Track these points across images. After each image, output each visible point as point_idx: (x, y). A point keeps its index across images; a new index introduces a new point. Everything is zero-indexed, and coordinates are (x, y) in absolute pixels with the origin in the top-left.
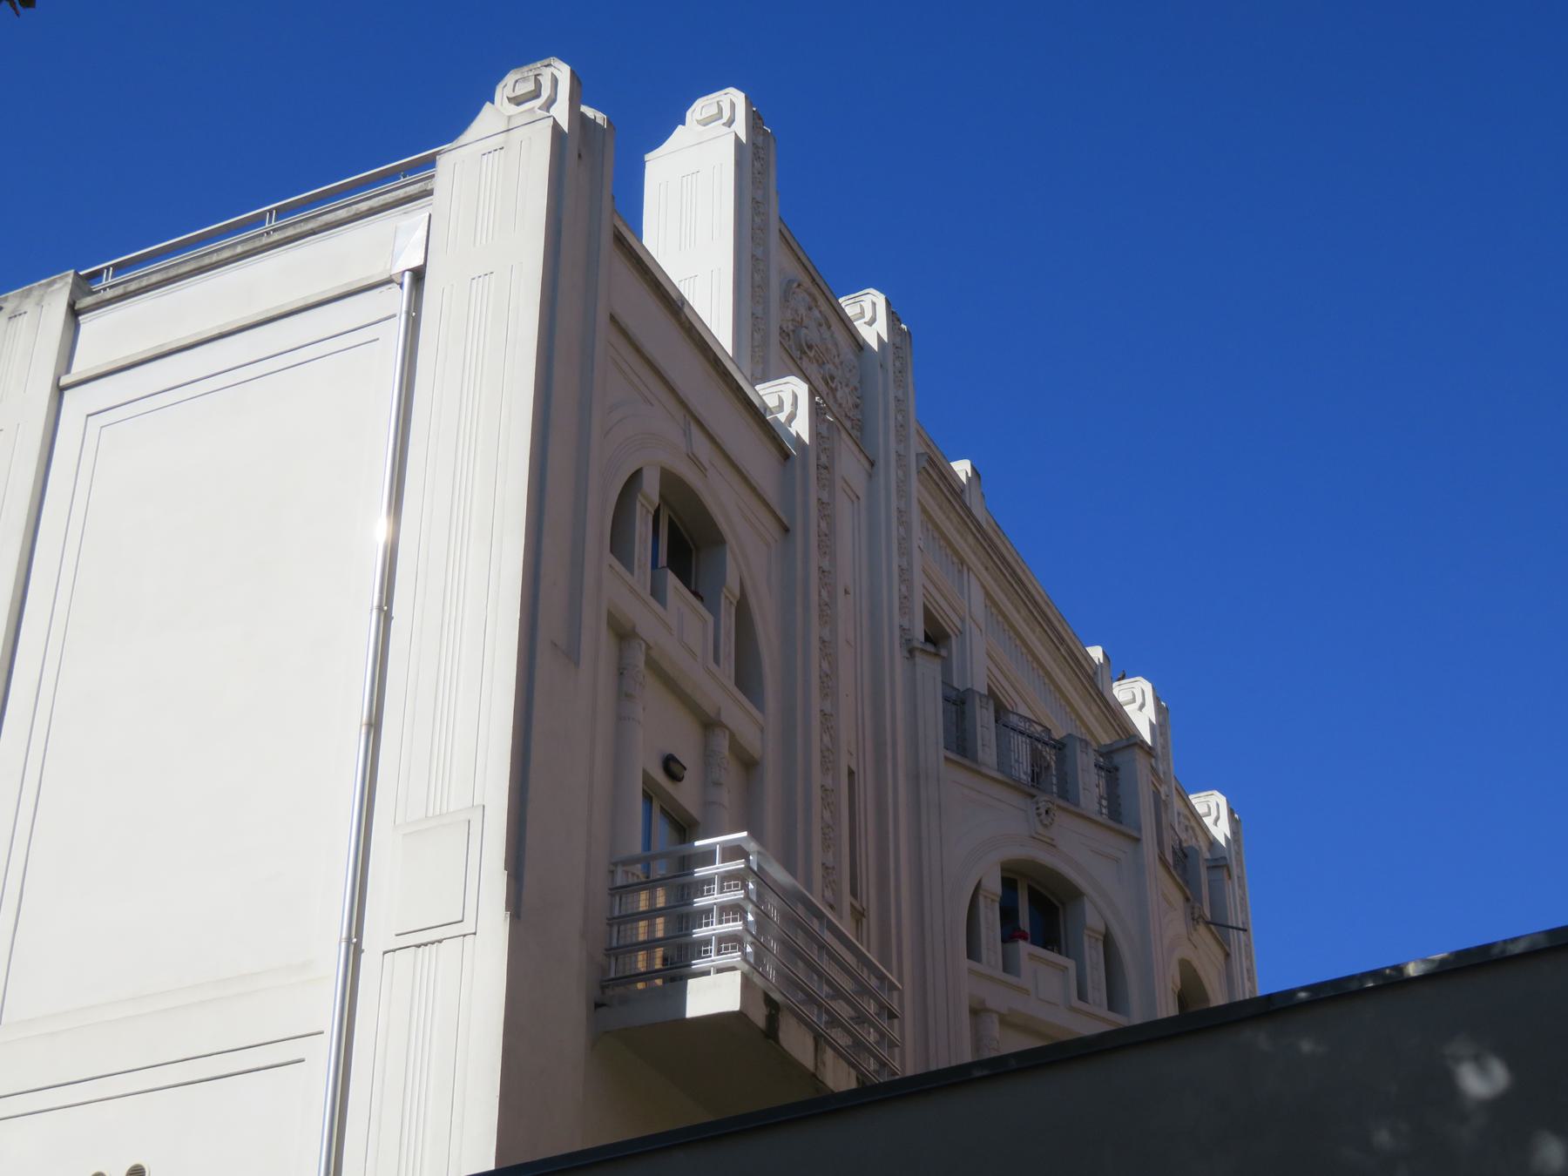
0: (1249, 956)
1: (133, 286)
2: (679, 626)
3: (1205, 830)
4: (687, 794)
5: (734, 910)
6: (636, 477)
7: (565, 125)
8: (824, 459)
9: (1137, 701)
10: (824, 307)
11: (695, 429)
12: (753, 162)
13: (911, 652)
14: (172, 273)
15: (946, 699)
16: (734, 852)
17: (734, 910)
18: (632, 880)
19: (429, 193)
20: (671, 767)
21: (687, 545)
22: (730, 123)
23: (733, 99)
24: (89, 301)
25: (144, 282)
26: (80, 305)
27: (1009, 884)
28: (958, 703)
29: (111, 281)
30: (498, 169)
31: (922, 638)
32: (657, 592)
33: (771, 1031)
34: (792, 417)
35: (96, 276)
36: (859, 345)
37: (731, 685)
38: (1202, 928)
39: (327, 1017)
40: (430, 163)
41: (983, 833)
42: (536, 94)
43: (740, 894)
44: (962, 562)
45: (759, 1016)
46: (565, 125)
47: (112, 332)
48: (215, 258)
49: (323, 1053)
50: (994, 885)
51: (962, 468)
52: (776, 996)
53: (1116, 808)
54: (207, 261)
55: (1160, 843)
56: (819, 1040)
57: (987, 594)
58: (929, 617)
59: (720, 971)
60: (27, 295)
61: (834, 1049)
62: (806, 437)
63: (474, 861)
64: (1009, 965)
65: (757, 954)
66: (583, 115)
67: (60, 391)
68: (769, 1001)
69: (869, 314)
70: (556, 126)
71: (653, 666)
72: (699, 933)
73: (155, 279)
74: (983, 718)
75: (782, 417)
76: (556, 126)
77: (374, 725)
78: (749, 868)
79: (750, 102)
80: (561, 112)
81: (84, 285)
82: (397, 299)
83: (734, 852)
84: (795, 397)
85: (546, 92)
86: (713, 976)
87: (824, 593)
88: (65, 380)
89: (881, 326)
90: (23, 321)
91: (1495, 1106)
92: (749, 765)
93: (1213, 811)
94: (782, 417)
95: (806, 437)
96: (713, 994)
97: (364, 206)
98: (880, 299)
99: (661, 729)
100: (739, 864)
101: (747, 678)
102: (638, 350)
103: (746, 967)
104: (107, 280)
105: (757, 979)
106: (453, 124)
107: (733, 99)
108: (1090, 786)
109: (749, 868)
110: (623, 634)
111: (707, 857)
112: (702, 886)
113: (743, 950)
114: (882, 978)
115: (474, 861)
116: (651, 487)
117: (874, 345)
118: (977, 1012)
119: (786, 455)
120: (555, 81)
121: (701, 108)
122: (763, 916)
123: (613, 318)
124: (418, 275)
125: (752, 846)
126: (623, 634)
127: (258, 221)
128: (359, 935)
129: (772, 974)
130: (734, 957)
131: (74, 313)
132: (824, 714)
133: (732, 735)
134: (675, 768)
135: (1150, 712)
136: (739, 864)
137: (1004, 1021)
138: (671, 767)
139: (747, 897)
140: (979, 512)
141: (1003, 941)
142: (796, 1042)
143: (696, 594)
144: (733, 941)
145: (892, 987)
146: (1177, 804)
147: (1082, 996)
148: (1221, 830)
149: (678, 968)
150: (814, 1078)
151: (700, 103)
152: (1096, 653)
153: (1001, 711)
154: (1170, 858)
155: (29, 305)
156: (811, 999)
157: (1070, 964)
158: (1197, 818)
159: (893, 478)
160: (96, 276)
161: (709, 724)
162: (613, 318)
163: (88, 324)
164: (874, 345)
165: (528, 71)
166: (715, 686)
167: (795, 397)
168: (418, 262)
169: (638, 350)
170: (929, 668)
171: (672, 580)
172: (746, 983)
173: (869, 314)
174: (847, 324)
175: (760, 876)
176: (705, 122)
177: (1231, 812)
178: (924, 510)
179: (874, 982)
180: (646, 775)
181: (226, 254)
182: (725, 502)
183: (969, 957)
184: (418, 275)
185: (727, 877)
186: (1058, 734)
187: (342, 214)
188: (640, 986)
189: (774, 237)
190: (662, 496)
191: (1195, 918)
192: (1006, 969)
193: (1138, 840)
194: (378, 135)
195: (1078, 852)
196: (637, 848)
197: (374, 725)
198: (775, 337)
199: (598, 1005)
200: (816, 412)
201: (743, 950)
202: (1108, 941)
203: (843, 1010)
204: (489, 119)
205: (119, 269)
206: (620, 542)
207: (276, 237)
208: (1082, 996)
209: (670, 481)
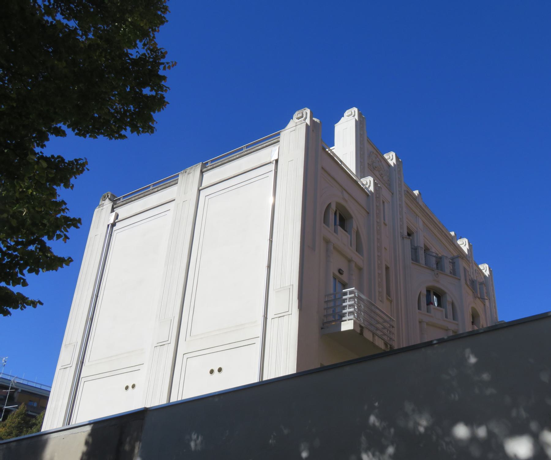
0: (495, 303)
1: (215, 166)
2: (341, 238)
3: (483, 273)
4: (344, 278)
5: (350, 306)
6: (330, 204)
7: (309, 124)
8: (377, 196)
9: (464, 244)
10: (380, 157)
11: (344, 192)
12: (359, 125)
13: (403, 238)
14: (223, 162)
15: (412, 248)
16: (351, 293)
17: (350, 306)
18: (330, 299)
19: (279, 141)
20: (340, 272)
21: (343, 220)
22: (354, 116)
23: (355, 110)
24: (205, 169)
25: (217, 165)
26: (203, 170)
27: (428, 291)
28: (415, 250)
29: (210, 164)
30: (293, 137)
31: (406, 234)
32: (336, 231)
33: (361, 333)
34: (369, 186)
35: (207, 163)
36: (389, 165)
37: (355, 251)
38: (477, 299)
39: (260, 334)
40: (279, 134)
41: (422, 279)
42: (302, 117)
43: (353, 302)
44: (417, 215)
45: (358, 330)
46: (309, 124)
47: (210, 177)
48: (232, 158)
49: (259, 342)
50: (424, 292)
51: (416, 192)
52: (363, 325)
53: (454, 272)
54: (230, 159)
55: (466, 280)
56: (374, 334)
57: (424, 222)
58: (408, 228)
59: (349, 320)
60: (192, 168)
61: (378, 336)
62: (373, 191)
63: (291, 298)
64: (428, 311)
65: (358, 316)
66: (314, 120)
67: (199, 191)
68: (361, 326)
69: (391, 158)
70: (307, 124)
71: (335, 248)
72: (344, 311)
73: (219, 164)
74: (421, 253)
75: (367, 186)
76: (307, 124)
77: (269, 267)
78: (355, 296)
79: (359, 111)
80: (308, 121)
81: (204, 166)
82: (273, 166)
83: (351, 293)
84: (370, 181)
85: (304, 116)
86: (347, 321)
87: (378, 228)
88: (200, 188)
89: (394, 161)
90: (191, 175)
91: (476, 364)
92: (360, 269)
93: (485, 269)
94: (367, 186)
95: (373, 191)
96: (347, 325)
97: (265, 145)
98: (394, 154)
99: (337, 262)
100: (353, 295)
101: (359, 249)
102: (329, 175)
103: (355, 319)
104: (209, 164)
105: (358, 322)
106: (283, 124)
107: (355, 110)
108: (448, 267)
109: (355, 296)
110: (327, 242)
111: (345, 294)
112: (344, 301)
113: (354, 315)
114: (390, 318)
115: (291, 298)
116: (333, 207)
117: (393, 165)
118: (420, 322)
119: (368, 195)
120: (306, 114)
121: (347, 113)
122: (359, 307)
123: (323, 168)
124: (277, 161)
125: (356, 291)
126: (327, 242)
127: (242, 149)
128: (267, 315)
129: (362, 320)
130: (352, 317)
131: (202, 173)
132: (378, 256)
133: (356, 263)
134: (341, 272)
135: (467, 246)
136: (353, 295)
137: (427, 324)
138: (340, 272)
139: (355, 303)
140: (421, 203)
141: (427, 305)
142: (368, 335)
143: (345, 231)
144: (350, 313)
145: (393, 320)
146: (475, 268)
147: (446, 317)
148: (487, 273)
149: (340, 318)
150: (373, 344)
151: (347, 111)
152: (453, 233)
153: (426, 249)
154: (469, 283)
155: (192, 171)
156: (371, 324)
157: (444, 310)
158: (481, 271)
159: (398, 197)
160: (207, 163)
161: (350, 261)
162: (323, 168)
163: (206, 175)
164: (393, 165)
165: (300, 111)
166: (351, 252)
167: (370, 181)
168: (277, 158)
169: (329, 175)
170: (407, 242)
171: (339, 228)
172: (355, 323)
173: (391, 158)
174: (386, 161)
175: (359, 298)
176: (348, 116)
177: (489, 268)
178: (406, 204)
179: (388, 319)
180: (334, 274)
181: (235, 157)
182: (352, 208)
183: (419, 309)
184: (277, 161)
185: (350, 298)
186: (440, 255)
187: (260, 147)
188: (333, 323)
189: (366, 141)
190: (336, 207)
191: (475, 297)
192: (427, 312)
193: (460, 279)
194: (267, 129)
195: (444, 283)
196: (331, 291)
197: (269, 267)
198: (366, 165)
199: (322, 328)
200: (375, 184)
201: (354, 315)
202: (453, 304)
203: (379, 326)
204: (292, 124)
205: (212, 161)
206: (326, 220)
207: (246, 153)
208: (446, 317)
209: (338, 205)
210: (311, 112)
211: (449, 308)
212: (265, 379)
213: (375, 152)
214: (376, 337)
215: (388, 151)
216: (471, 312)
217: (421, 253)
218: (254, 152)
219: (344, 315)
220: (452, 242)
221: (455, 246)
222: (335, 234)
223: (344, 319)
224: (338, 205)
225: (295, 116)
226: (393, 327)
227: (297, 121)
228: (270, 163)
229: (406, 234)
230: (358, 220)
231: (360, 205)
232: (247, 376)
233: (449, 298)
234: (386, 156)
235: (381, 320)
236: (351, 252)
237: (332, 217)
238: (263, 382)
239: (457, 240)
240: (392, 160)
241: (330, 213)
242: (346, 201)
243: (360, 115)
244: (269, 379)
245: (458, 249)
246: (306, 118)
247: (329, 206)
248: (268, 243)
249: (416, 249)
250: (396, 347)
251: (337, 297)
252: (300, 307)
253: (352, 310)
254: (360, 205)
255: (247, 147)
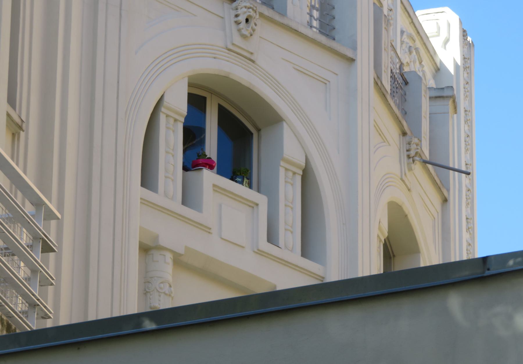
0: (470, 202)
3: (431, 54)
27: (197, 103)
38: (418, 167)
50: (179, 104)
114: (38, 204)
118: (145, 250)
137: (179, 262)
141: (185, 169)
147: (272, 237)
154: (387, 84)
157: (262, 200)
177: (464, 34)
179: (29, 209)
183: (145, 183)
191: (411, 156)
193: (352, 60)
202: (307, 177)
208: (272, 237)
211: (289, 192)
226: (47, 248)
233: (289, 147)
250: (430, 256)
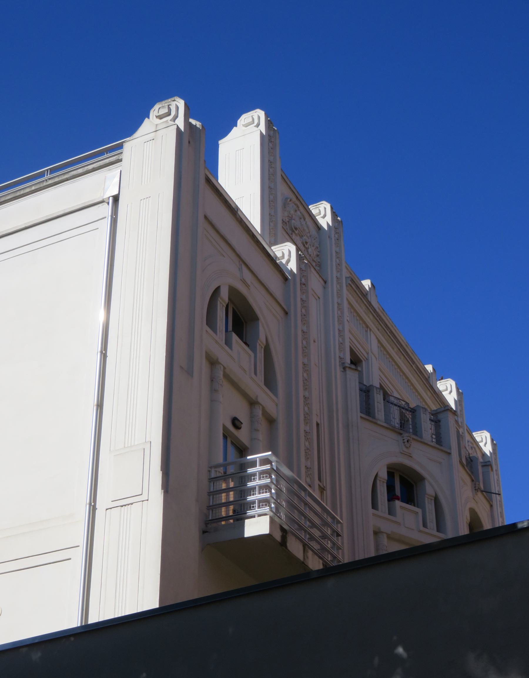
2: (238, 358)
3: (480, 449)
4: (243, 435)
5: (266, 488)
6: (218, 289)
7: (182, 128)
9: (448, 390)
10: (301, 208)
11: (244, 267)
12: (268, 143)
13: (344, 368)
15: (361, 390)
16: (265, 461)
18: (219, 475)
19: (120, 161)
20: (236, 423)
21: (241, 321)
22: (258, 125)
23: (259, 114)
27: (391, 474)
28: (366, 392)
31: (349, 362)
32: (228, 342)
33: (283, 543)
34: (288, 261)
36: (319, 227)
38: (479, 494)
40: (120, 146)
41: (378, 451)
42: (169, 114)
43: (268, 480)
44: (367, 327)
45: (278, 536)
46: (182, 128)
48: (22, 192)
50: (384, 475)
51: (367, 283)
52: (286, 527)
53: (439, 439)
54: (18, 194)
56: (306, 547)
57: (379, 341)
58: (352, 352)
59: (260, 515)
61: (312, 551)
62: (295, 270)
64: (391, 511)
65: (277, 508)
66: (190, 123)
68: (282, 529)
69: (323, 213)
70: (178, 129)
71: (227, 376)
74: (378, 398)
76: (178, 129)
77: (100, 406)
79: (267, 116)
80: (180, 122)
82: (106, 210)
83: (265, 461)
85: (173, 113)
86: (256, 518)
92: (271, 421)
95: (295, 270)
96: (257, 526)
98: (328, 206)
99: (231, 405)
100: (268, 467)
101: (269, 381)
103: (272, 514)
105: (277, 519)
106: (131, 127)
108: (427, 429)
110: (213, 362)
111: (253, 464)
113: (270, 506)
116: (224, 294)
118: (376, 533)
119: (286, 279)
120: (177, 108)
121: (244, 119)
122: (279, 491)
123: (206, 217)
124: (116, 199)
125: (273, 459)
126: (213, 362)
127: (42, 175)
129: (283, 517)
130: (266, 509)
134: (236, 422)
135: (454, 395)
136: (268, 467)
138: (236, 423)
141: (389, 500)
142: (295, 547)
143: (246, 343)
144: (264, 502)
145: (338, 522)
146: (467, 437)
147: (425, 525)
148: (488, 449)
150: (303, 564)
151: (244, 116)
152: (429, 368)
153: (386, 395)
156: (301, 528)
157: (419, 510)
161: (252, 403)
162: (206, 217)
164: (325, 227)
165: (165, 103)
166: (255, 386)
168: (116, 192)
170: (352, 376)
171: (235, 337)
173: (323, 213)
174: (313, 218)
176: (246, 125)
177: (492, 440)
178: (349, 303)
180: (225, 428)
181: (27, 190)
182: (258, 300)
184: (116, 199)
185: (262, 473)
187: (80, 171)
188: (223, 523)
190: (229, 299)
191: (476, 489)
192: (389, 514)
193: (449, 454)
195: (422, 459)
196: (220, 460)
197: (100, 406)
201: (270, 506)
202: (436, 500)
203: (316, 533)
204: (148, 126)
206: (211, 320)
208: (425, 525)
209: (233, 292)
210: (187, 107)
211: (430, 507)
212: (93, 619)
213: (294, 199)
214: (310, 553)
215: (316, 200)
216: (469, 519)
217: (378, 398)
218: (67, 180)
219: (250, 505)
220: (428, 383)
221: (435, 391)
222: (227, 348)
223: (250, 513)
224: (233, 292)
225: (154, 112)
226: (338, 535)
227: (158, 121)
228: (102, 202)
229: (348, 361)
230: (269, 325)
231: (271, 295)
232: (60, 616)
234: (314, 209)
235: (317, 521)
236: (255, 386)
237: (221, 313)
238: (87, 626)
239: (437, 380)
240: (324, 217)
241: (220, 305)
242: (247, 286)
243: (269, 124)
244: (101, 620)
245: (438, 396)
246: (176, 117)
247: (217, 291)
248: (98, 357)
249: (368, 391)
251: (228, 473)
252: (166, 486)
253: (267, 495)
254: (271, 295)
255: (52, 171)
